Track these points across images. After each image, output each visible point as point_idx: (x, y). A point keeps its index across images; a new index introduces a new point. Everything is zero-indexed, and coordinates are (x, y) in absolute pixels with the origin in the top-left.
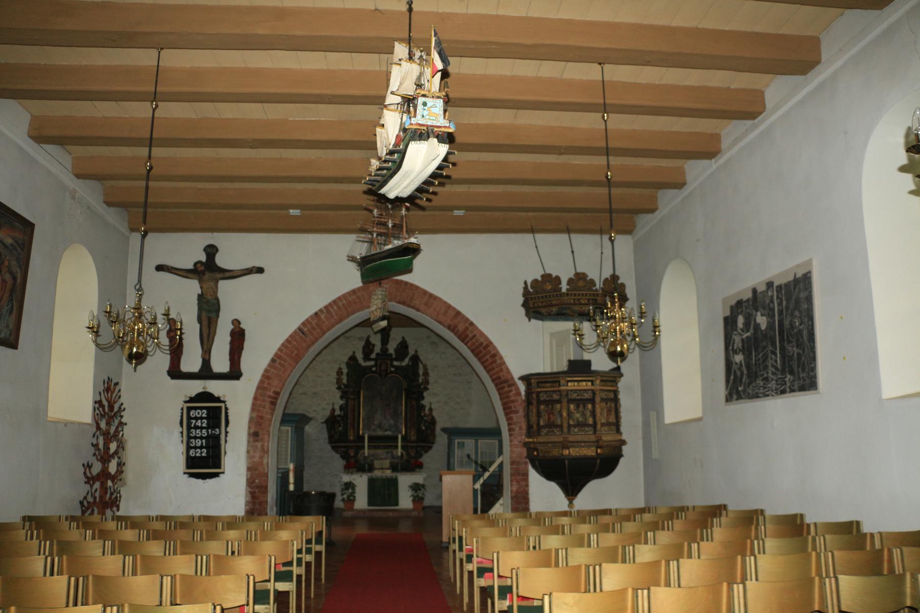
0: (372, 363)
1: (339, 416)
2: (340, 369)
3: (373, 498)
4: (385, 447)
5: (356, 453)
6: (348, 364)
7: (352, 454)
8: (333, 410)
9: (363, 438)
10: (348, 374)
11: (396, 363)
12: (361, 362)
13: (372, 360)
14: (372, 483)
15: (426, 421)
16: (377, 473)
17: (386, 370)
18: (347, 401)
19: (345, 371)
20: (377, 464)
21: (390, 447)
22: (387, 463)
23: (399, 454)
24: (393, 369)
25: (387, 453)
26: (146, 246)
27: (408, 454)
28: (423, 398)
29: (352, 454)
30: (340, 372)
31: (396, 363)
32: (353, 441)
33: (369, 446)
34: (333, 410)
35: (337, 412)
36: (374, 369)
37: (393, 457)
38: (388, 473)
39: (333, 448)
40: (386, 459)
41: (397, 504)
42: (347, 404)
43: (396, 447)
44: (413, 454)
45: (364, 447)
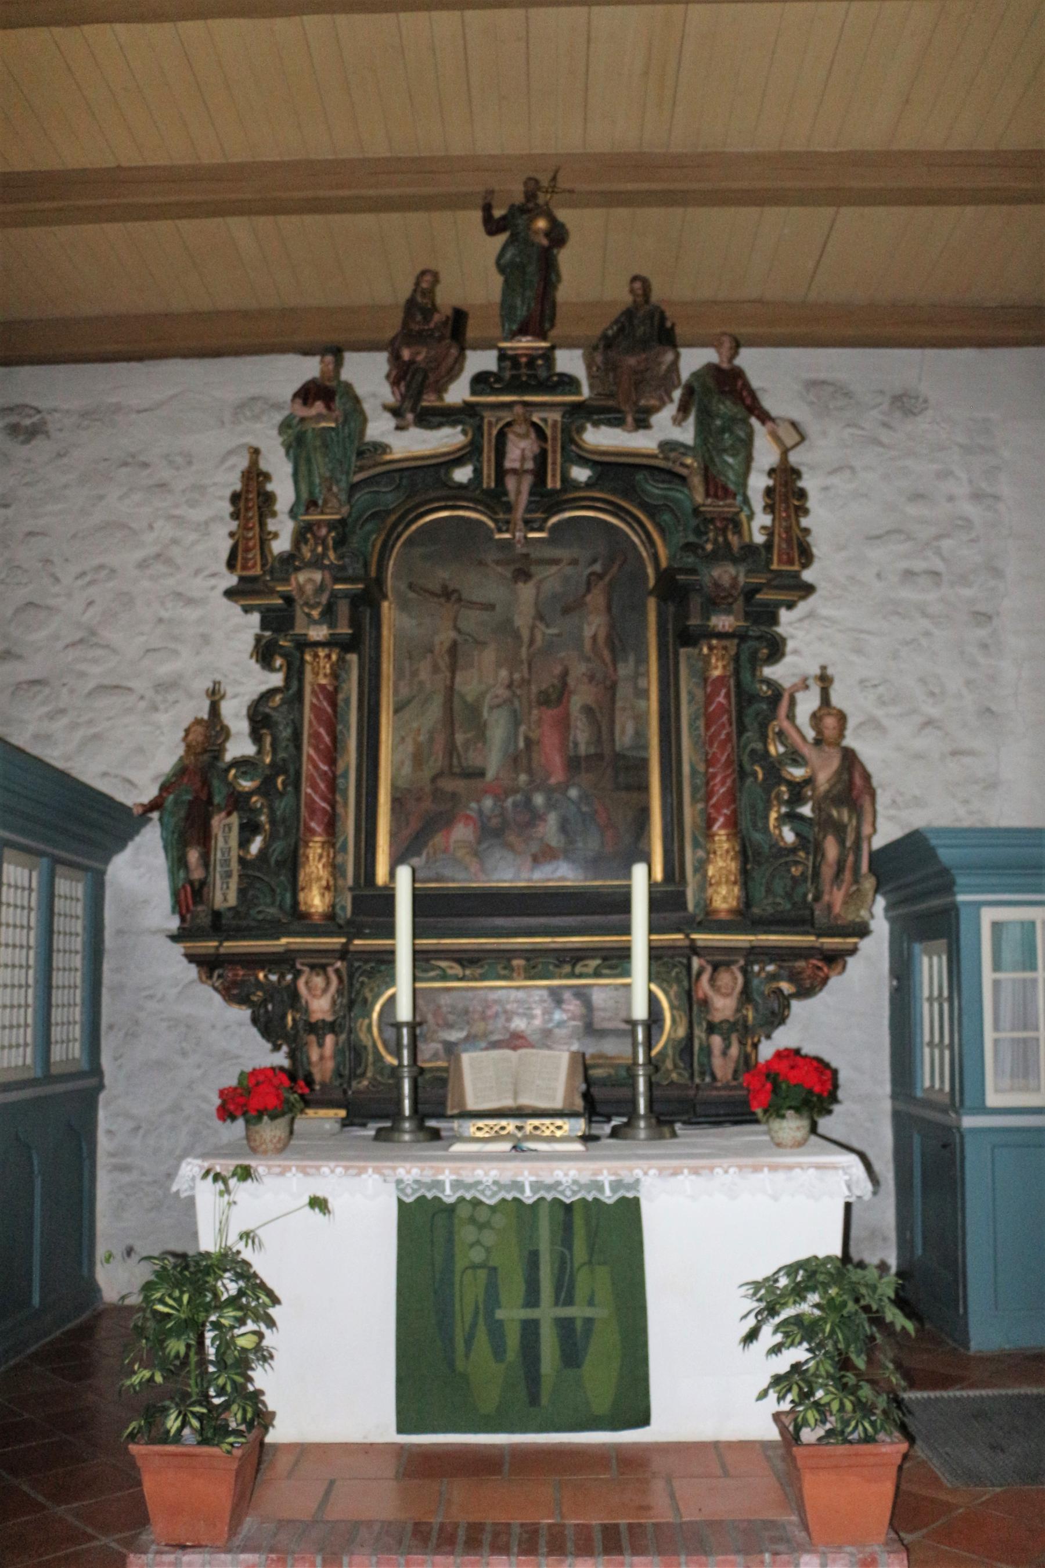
0: (448, 438)
1: (243, 764)
2: (255, 477)
3: (429, 1368)
4: (537, 964)
5: (352, 1003)
6: (297, 442)
7: (321, 1007)
8: (211, 731)
9: (388, 898)
10: (929, 1398)
11: (600, 438)
12: (379, 427)
13: (448, 416)
14: (426, 1230)
15: (798, 792)
16: (475, 1168)
17: (540, 473)
18: (295, 673)
19: (283, 490)
20: (480, 1077)
21: (572, 959)
22: (551, 1078)
23: (640, 1011)
24: (581, 474)
25: (556, 996)
26: (829, 1135)
27: (691, 1004)
28: (776, 649)
29: (321, 1007)
30: (252, 499)
31: (600, 438)
32: (330, 922)
33: (419, 956)
34: (211, 731)
35: (240, 746)
36: (462, 474)
37: (590, 1029)
38: (567, 1167)
39: (208, 965)
40: (546, 1038)
41: (643, 1419)
42: (292, 692)
43: (617, 960)
44: (724, 1007)
45: (388, 958)
